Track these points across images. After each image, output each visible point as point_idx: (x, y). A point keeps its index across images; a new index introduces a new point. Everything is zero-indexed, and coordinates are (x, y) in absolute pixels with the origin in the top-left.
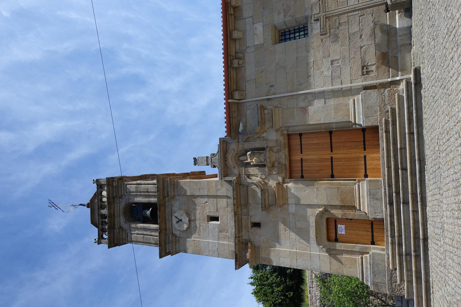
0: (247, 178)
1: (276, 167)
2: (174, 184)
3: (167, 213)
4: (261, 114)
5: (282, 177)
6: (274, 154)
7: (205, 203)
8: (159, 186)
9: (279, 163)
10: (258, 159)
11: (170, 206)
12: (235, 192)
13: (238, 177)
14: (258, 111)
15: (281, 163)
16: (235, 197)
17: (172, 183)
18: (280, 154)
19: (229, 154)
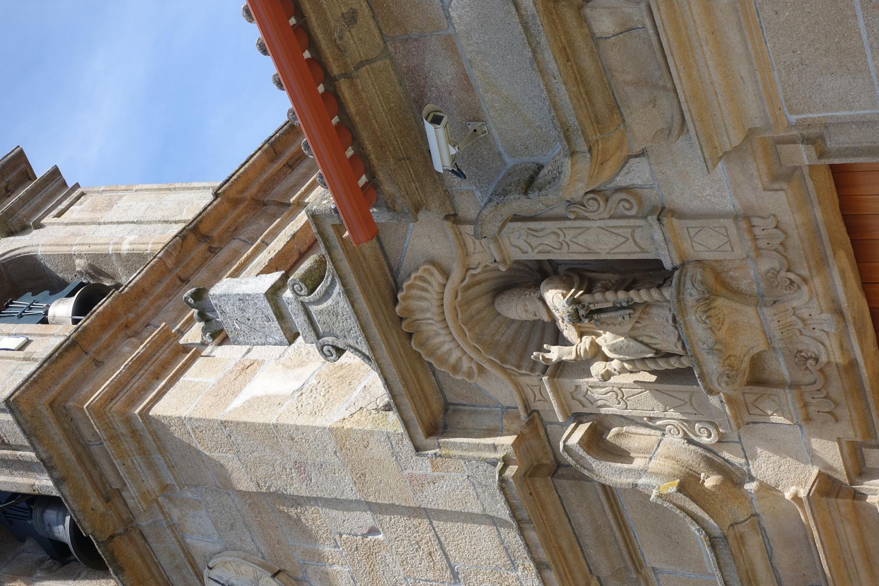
0: (588, 457)
1: (781, 385)
2: (134, 433)
3: (164, 560)
4: (567, 53)
5: (839, 440)
6: (750, 311)
7: (364, 536)
8: (51, 457)
9: (801, 359)
10: (632, 343)
11: (168, 531)
12: (534, 536)
13: (526, 431)
14: (534, 52)
15: (817, 360)
16: (543, 555)
17: (122, 429)
18: (795, 304)
19: (415, 292)
